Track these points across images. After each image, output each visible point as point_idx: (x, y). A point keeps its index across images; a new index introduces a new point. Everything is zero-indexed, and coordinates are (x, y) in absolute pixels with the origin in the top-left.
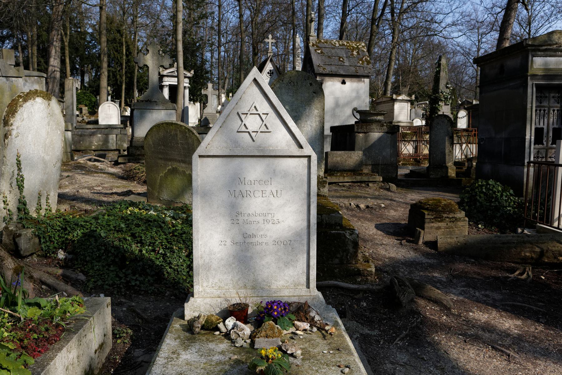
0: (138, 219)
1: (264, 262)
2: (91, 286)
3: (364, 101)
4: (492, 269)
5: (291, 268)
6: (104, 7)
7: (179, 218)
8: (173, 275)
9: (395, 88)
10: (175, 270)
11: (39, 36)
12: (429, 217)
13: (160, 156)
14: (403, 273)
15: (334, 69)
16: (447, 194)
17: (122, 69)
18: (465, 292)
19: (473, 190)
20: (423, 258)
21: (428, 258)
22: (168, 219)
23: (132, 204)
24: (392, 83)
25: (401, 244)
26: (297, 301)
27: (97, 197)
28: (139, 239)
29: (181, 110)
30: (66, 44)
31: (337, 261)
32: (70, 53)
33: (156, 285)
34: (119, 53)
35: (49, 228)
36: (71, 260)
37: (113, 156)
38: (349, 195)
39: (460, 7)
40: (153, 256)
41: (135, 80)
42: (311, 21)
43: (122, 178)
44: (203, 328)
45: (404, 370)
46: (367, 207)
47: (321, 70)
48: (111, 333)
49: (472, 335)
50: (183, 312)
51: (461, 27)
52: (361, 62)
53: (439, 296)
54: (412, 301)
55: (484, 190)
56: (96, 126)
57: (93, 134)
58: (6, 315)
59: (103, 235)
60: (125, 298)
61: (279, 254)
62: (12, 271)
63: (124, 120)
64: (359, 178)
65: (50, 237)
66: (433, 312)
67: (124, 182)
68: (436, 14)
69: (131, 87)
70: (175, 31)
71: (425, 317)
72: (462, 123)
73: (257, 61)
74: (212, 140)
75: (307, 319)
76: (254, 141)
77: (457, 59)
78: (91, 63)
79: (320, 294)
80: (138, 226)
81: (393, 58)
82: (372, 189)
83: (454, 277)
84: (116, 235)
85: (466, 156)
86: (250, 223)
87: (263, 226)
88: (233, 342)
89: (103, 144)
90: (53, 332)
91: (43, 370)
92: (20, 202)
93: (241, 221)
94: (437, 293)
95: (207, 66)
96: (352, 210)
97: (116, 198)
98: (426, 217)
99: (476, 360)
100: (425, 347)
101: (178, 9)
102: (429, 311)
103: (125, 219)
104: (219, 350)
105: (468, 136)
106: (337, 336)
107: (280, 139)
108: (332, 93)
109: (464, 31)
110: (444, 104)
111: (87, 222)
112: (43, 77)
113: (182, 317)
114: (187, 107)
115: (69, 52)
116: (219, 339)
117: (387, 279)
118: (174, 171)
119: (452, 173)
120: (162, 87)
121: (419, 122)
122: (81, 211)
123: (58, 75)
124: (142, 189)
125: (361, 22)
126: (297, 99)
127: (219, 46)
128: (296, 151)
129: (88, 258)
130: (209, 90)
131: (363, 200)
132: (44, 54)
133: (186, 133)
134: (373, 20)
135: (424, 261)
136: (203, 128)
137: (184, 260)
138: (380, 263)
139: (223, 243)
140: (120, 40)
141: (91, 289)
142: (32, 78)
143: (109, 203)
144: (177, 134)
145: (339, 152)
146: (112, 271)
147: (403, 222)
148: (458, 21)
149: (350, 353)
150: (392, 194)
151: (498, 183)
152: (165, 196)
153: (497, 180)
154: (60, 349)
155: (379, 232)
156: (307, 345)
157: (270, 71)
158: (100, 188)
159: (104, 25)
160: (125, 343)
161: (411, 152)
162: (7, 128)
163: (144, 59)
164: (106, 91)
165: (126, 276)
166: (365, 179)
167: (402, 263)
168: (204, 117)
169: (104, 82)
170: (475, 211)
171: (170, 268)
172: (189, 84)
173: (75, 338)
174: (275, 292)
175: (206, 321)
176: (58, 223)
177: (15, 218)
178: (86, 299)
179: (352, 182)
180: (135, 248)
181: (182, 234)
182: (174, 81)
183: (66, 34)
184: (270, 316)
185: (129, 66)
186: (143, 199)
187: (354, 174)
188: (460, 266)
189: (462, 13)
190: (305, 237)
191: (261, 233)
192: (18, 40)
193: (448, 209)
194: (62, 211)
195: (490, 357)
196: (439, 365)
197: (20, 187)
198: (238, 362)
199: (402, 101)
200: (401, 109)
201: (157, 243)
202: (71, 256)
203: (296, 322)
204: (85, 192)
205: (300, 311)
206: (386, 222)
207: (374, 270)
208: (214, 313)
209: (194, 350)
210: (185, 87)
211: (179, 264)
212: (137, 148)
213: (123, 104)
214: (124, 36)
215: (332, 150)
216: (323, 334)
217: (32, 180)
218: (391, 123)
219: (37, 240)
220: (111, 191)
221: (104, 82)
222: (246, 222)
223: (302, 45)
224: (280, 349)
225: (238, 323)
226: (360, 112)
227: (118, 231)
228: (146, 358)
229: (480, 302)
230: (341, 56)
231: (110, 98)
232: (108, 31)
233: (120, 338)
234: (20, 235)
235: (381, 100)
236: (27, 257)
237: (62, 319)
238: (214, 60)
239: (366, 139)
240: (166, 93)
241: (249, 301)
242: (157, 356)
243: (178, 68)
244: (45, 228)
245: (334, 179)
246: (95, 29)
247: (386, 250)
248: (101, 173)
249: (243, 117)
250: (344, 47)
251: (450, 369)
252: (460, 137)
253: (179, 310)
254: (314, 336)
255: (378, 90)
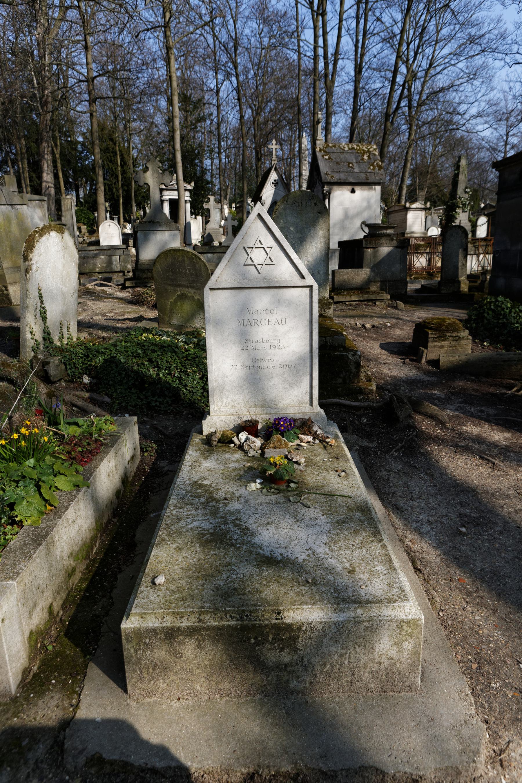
0: (153, 344)
1: (271, 384)
2: (116, 407)
3: (375, 211)
4: (491, 386)
5: (296, 388)
6: (94, 114)
7: (191, 343)
8: (188, 396)
9: (411, 192)
10: (190, 391)
11: (28, 148)
12: (432, 336)
13: (169, 282)
14: (404, 391)
15: (342, 176)
16: (457, 311)
17: (118, 181)
18: (461, 408)
19: (481, 307)
20: (424, 376)
21: (429, 376)
22: (181, 344)
23: (146, 330)
24: (407, 187)
25: (404, 363)
26: (302, 417)
27: (110, 323)
28: (155, 364)
29: (183, 227)
30: (58, 156)
31: (340, 380)
32: (63, 166)
33: (174, 406)
34: (113, 164)
35: (73, 355)
36: (95, 384)
37: (118, 278)
38: (354, 315)
39: (487, 94)
40: (169, 379)
41: (133, 195)
42: (318, 122)
43: (131, 302)
44: (219, 441)
45: (397, 476)
46: (373, 326)
47: (329, 179)
48: (139, 447)
49: (463, 446)
50: (202, 428)
51: (488, 119)
52: (372, 167)
53: (435, 412)
54: (410, 416)
55: (492, 307)
56: (98, 248)
57: (96, 256)
58: (51, 433)
59: (122, 360)
60: (148, 418)
61: (285, 376)
62: (45, 395)
63: (125, 237)
64: (366, 296)
65: (75, 364)
66: (428, 427)
67: (134, 307)
68: (459, 104)
69: (127, 199)
70: (172, 138)
71: (421, 431)
72: (482, 232)
73: (261, 167)
74: (221, 274)
75: (310, 433)
76: (259, 273)
77: (482, 155)
78: (85, 176)
79: (322, 411)
80: (154, 351)
81: (410, 158)
82: (380, 307)
83: (453, 394)
84: (134, 360)
85: (483, 268)
86: (258, 348)
87: (269, 351)
88: (246, 452)
89: (107, 266)
90: (94, 446)
91: (91, 475)
92: (44, 332)
93: (249, 348)
94: (433, 409)
95: (208, 177)
96: (358, 330)
97: (129, 324)
98: (430, 336)
99: (463, 467)
100: (418, 457)
101: (175, 114)
102: (425, 425)
103: (141, 345)
104: (234, 459)
105: (486, 245)
106: (337, 447)
107: (284, 271)
108: (341, 203)
109: (490, 123)
110: (461, 211)
111: (106, 349)
112: (44, 201)
113: (201, 432)
114: (189, 223)
115: (61, 165)
116: (233, 450)
117: (387, 396)
118: (183, 297)
119: (465, 287)
120: (162, 202)
121: (435, 231)
122: (99, 338)
123: (53, 191)
124: (153, 314)
125: (374, 116)
126: (302, 220)
127: (219, 153)
128: (299, 282)
129: (111, 382)
130: (211, 204)
131: (369, 320)
132: (36, 169)
133: (193, 259)
134: (387, 116)
135: (425, 380)
136: (207, 247)
137: (198, 383)
138: (382, 381)
139: (234, 367)
140: (113, 148)
141: (117, 410)
142: (34, 202)
143: (123, 329)
144: (184, 261)
145: (346, 270)
146: (134, 393)
147: (408, 341)
148: (484, 111)
149: (347, 460)
150: (399, 312)
151: (508, 299)
152: (176, 320)
153: (506, 296)
154: (102, 459)
155: (384, 352)
156: (310, 455)
157: (275, 181)
158: (112, 314)
159: (96, 135)
160: (151, 456)
161: (424, 265)
162: (27, 263)
163: (144, 177)
164: (104, 208)
165: (146, 397)
166: (372, 297)
167: (404, 382)
168: (207, 233)
169: (101, 198)
170: (482, 328)
171: (186, 389)
172: (190, 197)
173: (112, 450)
174: (281, 410)
175: (222, 436)
176: (81, 351)
177: (41, 347)
178: (115, 418)
179: (359, 301)
180: (153, 372)
181: (194, 358)
182: (174, 195)
183: (56, 145)
184: (278, 430)
185: (125, 178)
186: (155, 325)
187: (361, 293)
188: (460, 383)
189: (489, 101)
190: (308, 361)
191: (269, 357)
192: (7, 153)
193: (452, 328)
194: (82, 339)
195: (476, 465)
196: (429, 472)
197: (44, 319)
198: (250, 468)
199: (417, 209)
200: (416, 218)
201: (173, 367)
202: (94, 381)
203: (300, 436)
204: (98, 319)
205: (304, 425)
206: (391, 341)
207: (375, 388)
208: (228, 429)
209: (213, 459)
210: (186, 201)
211: (194, 386)
212: (143, 271)
213: (122, 220)
214: (117, 145)
215: (339, 268)
216: (324, 445)
217: (54, 311)
218: (403, 234)
219: (63, 367)
220: (123, 317)
221: (101, 198)
222: (255, 348)
223: (309, 147)
224: (286, 457)
225: (250, 437)
226: (369, 226)
227: (136, 357)
228: (171, 468)
229: (475, 417)
230: (351, 161)
231: (108, 215)
232: (101, 139)
233: (147, 451)
234: (48, 363)
235: (394, 208)
236: (55, 382)
237: (99, 435)
238: (214, 167)
239: (375, 254)
240: (166, 209)
241: (259, 418)
242: (182, 464)
243: (177, 180)
244: (69, 355)
245: (340, 298)
246: (85, 138)
247: (389, 369)
248: (110, 298)
249: (249, 251)
250: (354, 151)
251: (439, 475)
252: (477, 248)
253: (197, 427)
254: (316, 447)
255: (392, 195)
